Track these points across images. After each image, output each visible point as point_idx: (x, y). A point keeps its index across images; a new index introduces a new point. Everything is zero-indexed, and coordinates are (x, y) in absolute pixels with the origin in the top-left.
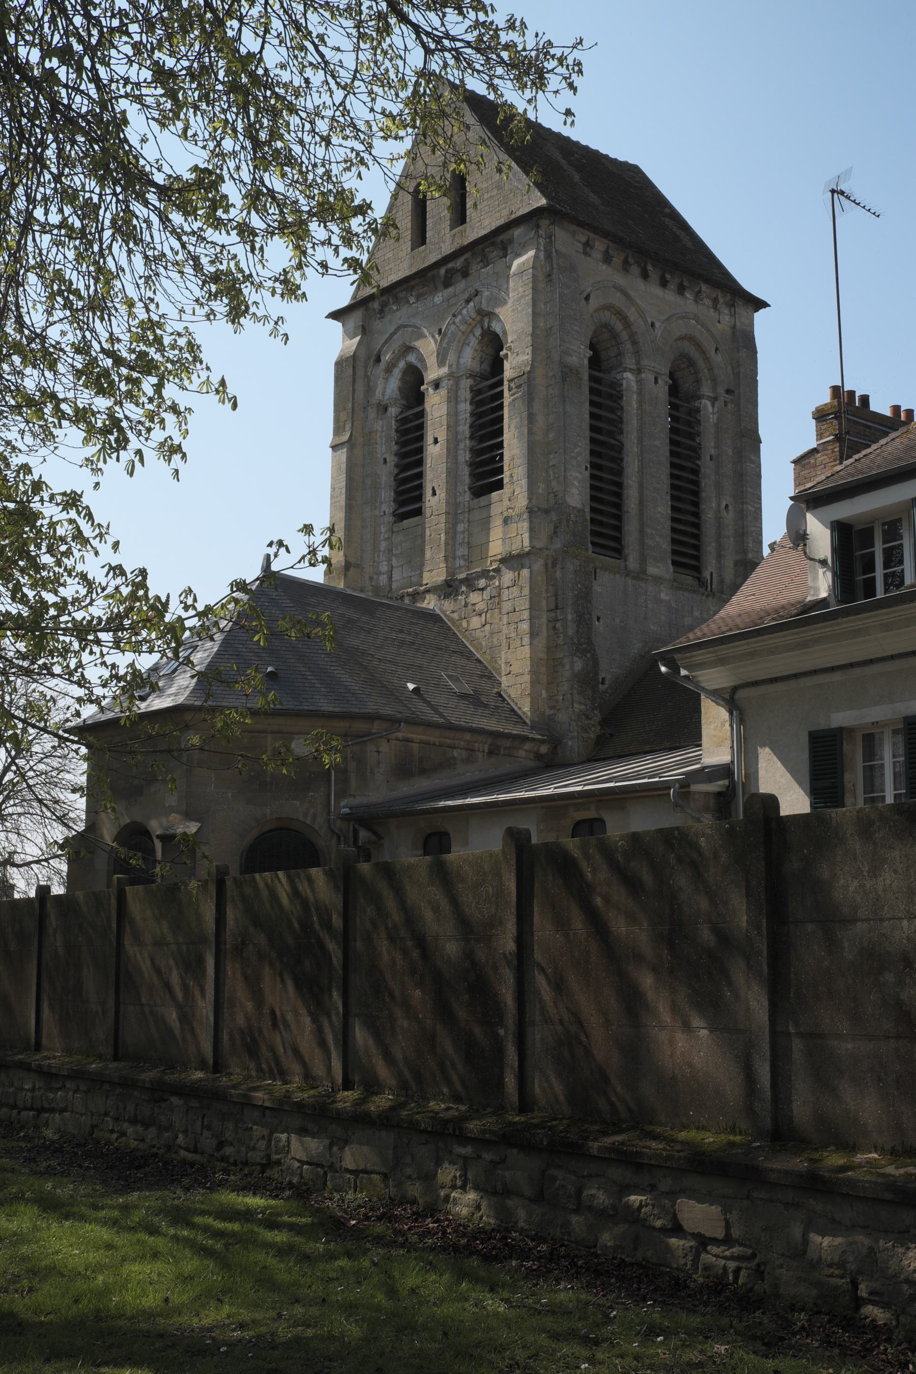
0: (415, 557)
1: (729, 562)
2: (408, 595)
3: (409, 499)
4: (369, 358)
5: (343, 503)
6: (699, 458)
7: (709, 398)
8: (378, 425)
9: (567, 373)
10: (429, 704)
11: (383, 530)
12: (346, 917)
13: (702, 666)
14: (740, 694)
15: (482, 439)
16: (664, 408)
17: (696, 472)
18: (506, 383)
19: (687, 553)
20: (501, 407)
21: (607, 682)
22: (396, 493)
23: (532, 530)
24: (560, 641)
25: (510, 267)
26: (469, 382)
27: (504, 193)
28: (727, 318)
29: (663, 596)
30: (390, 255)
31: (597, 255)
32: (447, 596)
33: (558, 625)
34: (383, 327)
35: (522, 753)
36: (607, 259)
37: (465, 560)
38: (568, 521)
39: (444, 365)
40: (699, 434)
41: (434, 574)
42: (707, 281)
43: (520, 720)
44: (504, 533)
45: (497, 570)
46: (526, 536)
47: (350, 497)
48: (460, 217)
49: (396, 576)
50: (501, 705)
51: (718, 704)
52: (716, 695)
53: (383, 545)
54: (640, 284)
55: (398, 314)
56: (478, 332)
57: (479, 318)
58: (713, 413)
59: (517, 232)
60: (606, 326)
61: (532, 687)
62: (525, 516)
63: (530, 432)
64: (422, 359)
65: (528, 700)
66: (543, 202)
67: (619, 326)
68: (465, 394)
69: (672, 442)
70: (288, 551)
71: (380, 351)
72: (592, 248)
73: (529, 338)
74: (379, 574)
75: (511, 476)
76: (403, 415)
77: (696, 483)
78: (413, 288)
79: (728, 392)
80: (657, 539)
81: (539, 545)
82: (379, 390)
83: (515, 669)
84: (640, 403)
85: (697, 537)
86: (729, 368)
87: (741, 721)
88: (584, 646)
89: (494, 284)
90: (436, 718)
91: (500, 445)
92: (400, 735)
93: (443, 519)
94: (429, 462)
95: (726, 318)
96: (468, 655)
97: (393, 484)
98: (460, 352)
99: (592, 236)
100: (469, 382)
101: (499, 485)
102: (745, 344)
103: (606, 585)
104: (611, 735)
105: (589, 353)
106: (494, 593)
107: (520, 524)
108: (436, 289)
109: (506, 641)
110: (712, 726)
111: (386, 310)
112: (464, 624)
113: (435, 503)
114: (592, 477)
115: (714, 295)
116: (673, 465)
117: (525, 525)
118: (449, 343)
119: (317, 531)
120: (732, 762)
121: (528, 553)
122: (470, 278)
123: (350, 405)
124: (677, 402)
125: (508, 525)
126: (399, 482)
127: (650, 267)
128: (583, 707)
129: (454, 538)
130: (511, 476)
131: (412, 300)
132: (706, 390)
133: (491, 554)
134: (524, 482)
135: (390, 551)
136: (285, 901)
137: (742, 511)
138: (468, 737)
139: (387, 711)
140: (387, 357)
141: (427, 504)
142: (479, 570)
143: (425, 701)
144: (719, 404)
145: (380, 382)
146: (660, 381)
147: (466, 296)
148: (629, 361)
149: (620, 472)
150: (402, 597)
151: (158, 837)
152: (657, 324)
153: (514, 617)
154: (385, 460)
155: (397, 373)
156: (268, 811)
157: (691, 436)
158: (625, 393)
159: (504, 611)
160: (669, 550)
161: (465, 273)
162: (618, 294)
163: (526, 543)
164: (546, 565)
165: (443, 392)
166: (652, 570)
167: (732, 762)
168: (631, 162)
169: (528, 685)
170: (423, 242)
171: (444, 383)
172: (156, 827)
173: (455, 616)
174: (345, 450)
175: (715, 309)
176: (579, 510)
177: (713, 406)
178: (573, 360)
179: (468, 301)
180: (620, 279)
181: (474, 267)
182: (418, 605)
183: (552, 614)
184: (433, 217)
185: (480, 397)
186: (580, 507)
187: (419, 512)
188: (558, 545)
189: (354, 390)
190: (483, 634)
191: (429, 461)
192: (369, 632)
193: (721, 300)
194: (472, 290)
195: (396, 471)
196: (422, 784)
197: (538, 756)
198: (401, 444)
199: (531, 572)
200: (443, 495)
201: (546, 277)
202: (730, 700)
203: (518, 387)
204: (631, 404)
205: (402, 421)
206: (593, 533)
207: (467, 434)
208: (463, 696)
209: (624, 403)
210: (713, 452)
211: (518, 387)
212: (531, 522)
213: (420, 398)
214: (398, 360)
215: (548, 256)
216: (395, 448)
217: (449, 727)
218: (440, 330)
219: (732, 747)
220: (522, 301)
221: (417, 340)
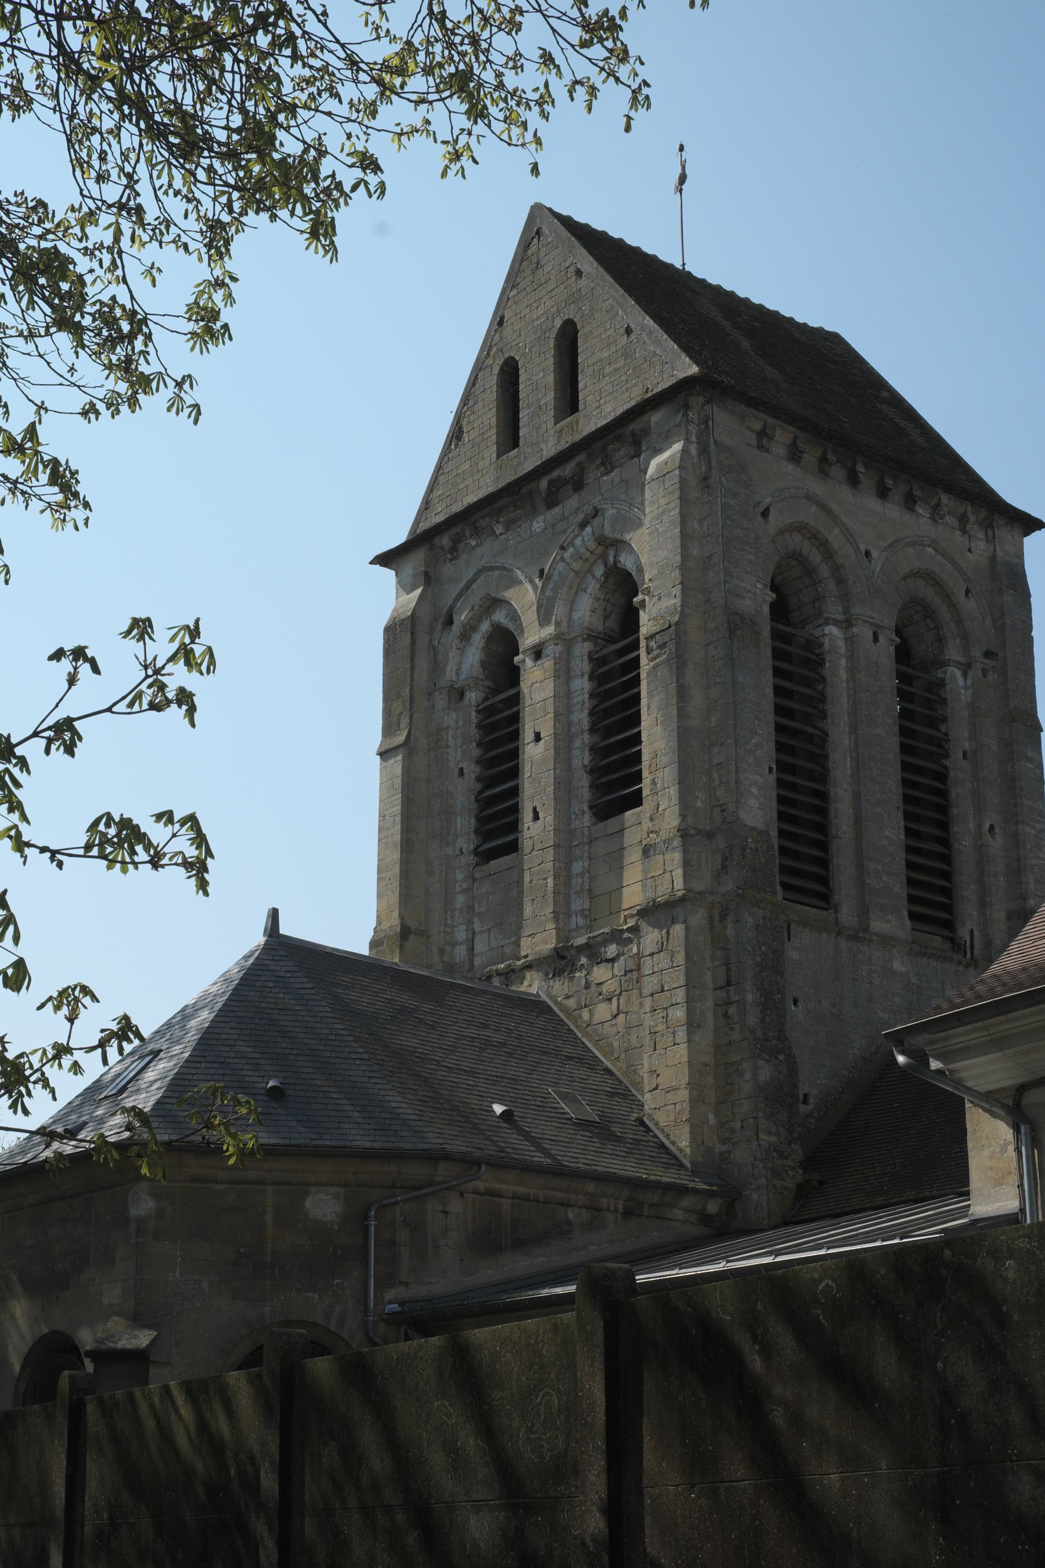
0: (509, 917)
1: (998, 912)
2: (499, 973)
3: (498, 827)
4: (436, 620)
5: (398, 838)
6: (946, 756)
7: (958, 665)
8: (450, 719)
9: (737, 625)
10: (527, 1136)
11: (460, 876)
12: (287, 1472)
13: (964, 1052)
14: (1032, 1097)
15: (608, 732)
16: (889, 683)
17: (942, 776)
18: (643, 644)
19: (932, 900)
20: (636, 681)
21: (811, 1100)
22: (478, 819)
23: (686, 864)
24: (736, 1036)
25: (645, 471)
26: (588, 646)
27: (633, 361)
28: (982, 545)
29: (897, 966)
30: (466, 466)
31: (779, 449)
32: (558, 973)
33: (732, 1011)
34: (457, 572)
35: (678, 1214)
36: (794, 455)
37: (586, 917)
38: (743, 849)
39: (548, 623)
40: (944, 720)
41: (539, 939)
42: (949, 489)
43: (673, 1161)
44: (645, 871)
45: (635, 930)
46: (678, 873)
47: (407, 829)
48: (569, 401)
49: (480, 946)
50: (644, 1137)
51: (994, 1115)
52: (991, 1100)
53: (460, 900)
54: (846, 493)
55: (479, 551)
56: (599, 571)
57: (600, 549)
58: (966, 688)
59: (655, 418)
60: (796, 555)
61: (692, 1108)
62: (676, 842)
63: (682, 714)
64: (515, 617)
65: (687, 1129)
66: (694, 369)
67: (815, 557)
68: (581, 664)
69: (903, 731)
70: (96, 670)
71: (451, 608)
72: (771, 439)
73: (677, 572)
74: (454, 944)
75: (654, 782)
76: (488, 703)
77: (944, 794)
78: (499, 511)
79: (988, 654)
80: (885, 878)
81: (698, 886)
82: (451, 667)
83: (664, 1081)
84: (852, 671)
85: (946, 875)
86: (988, 619)
87: (1034, 1142)
88: (774, 1042)
89: (623, 497)
90: (539, 1158)
91: (637, 739)
92: (481, 1185)
93: (550, 854)
94: (527, 771)
95: (980, 545)
96: (592, 1063)
97: (474, 806)
98: (573, 602)
99: (770, 420)
100: (588, 646)
101: (636, 800)
102: (1012, 584)
103: (805, 949)
104: (821, 1183)
105: (771, 596)
106: (631, 965)
107: (668, 856)
109: (651, 1038)
110: (986, 1153)
111: (461, 546)
112: (585, 1015)
113: (537, 831)
114: (780, 783)
115: (961, 511)
116: (905, 766)
117: (677, 856)
118: (555, 590)
119: (161, 632)
120: (1022, 1210)
121: (682, 900)
123: (407, 690)
124: (909, 671)
125: (650, 856)
126: (485, 803)
127: (860, 468)
128: (773, 1139)
129: (567, 883)
130: (654, 782)
131: (499, 529)
132: (953, 652)
133: (625, 906)
134: (673, 791)
135: (470, 908)
136: (182, 1440)
138: (591, 1187)
139: (458, 1146)
140: (462, 617)
141: (526, 834)
142: (606, 930)
143: (521, 1131)
144: (974, 673)
145: (453, 653)
146: (882, 639)
147: (580, 517)
148: (834, 609)
149: (824, 777)
150: (489, 978)
151: (88, 1354)
152: (875, 554)
153: (662, 1000)
155: (478, 639)
157: (933, 722)
158: (828, 658)
159: (646, 991)
160: (904, 895)
162: (814, 508)
163: (679, 884)
164: (711, 918)
165: (547, 663)
166: (878, 926)
167: (1022, 1210)
168: (829, 328)
169: (686, 1105)
170: (515, 444)
171: (549, 650)
172: (86, 1338)
173: (571, 1003)
174: (400, 757)
175: (964, 531)
176: (761, 833)
177: (965, 676)
178: (746, 605)
179: (583, 525)
180: (817, 487)
181: (591, 477)
182: (514, 988)
183: (722, 994)
184: (529, 406)
185: (605, 668)
186: (761, 826)
187: (513, 847)
188: (728, 886)
189: (413, 668)
190: (614, 1030)
191: (527, 768)
192: (433, 1027)
193: (972, 518)
194: (588, 509)
195: (478, 787)
196: (518, 1264)
197: (705, 1219)
198: (485, 745)
199: (687, 929)
200: (550, 819)
201: (698, 482)
202: (1014, 1106)
203: (662, 646)
204: (838, 671)
205: (486, 711)
206: (783, 869)
207: (586, 724)
208: (584, 1124)
209: (826, 671)
210: (967, 746)
211: (662, 646)
212: (685, 852)
213: (513, 676)
214: (480, 621)
215: (704, 450)
216: (476, 752)
217: (560, 1172)
218: (542, 571)
219: (1021, 1186)
220: (665, 518)
221: (508, 587)
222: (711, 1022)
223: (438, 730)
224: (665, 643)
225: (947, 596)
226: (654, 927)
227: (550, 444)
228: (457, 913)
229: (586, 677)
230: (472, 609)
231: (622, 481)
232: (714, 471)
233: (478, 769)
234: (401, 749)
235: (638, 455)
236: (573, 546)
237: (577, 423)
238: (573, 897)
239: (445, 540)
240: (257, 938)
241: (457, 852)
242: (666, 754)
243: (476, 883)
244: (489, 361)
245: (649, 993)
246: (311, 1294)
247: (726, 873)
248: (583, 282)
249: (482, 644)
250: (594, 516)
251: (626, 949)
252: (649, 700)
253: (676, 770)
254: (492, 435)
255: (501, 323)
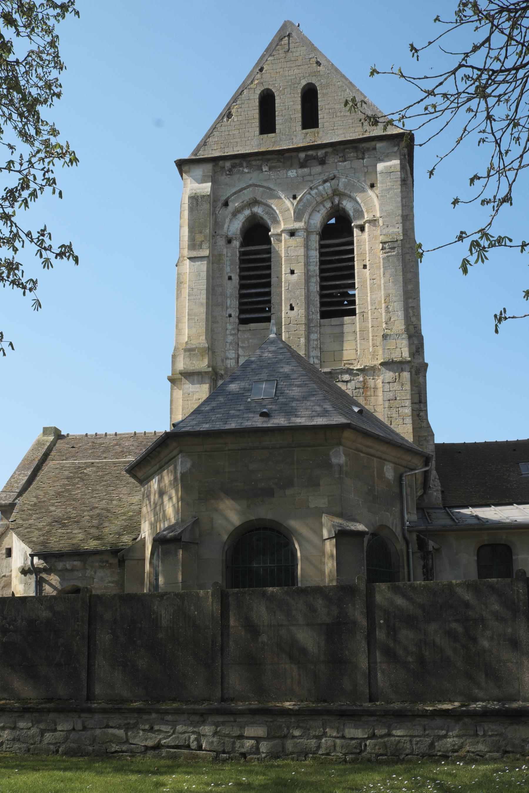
56: (328, 205)
71: (228, 198)
78: (269, 160)
108: (291, 167)
122: (325, 166)
140: (235, 204)
179: (325, 182)
181: (331, 160)
183: (417, 406)
224: (395, 247)
226: (390, 370)
227: (298, 138)
228: (228, 344)
230: (243, 202)
231: (351, 168)
234: (206, 259)
235: (363, 159)
236: (317, 189)
237: (318, 133)
239: (228, 164)
241: (227, 315)
242: (396, 296)
243: (240, 333)
245: (387, 399)
247: (419, 355)
248: (321, 68)
249: (243, 220)
250: (333, 179)
251: (355, 378)
252: (384, 270)
253: (402, 305)
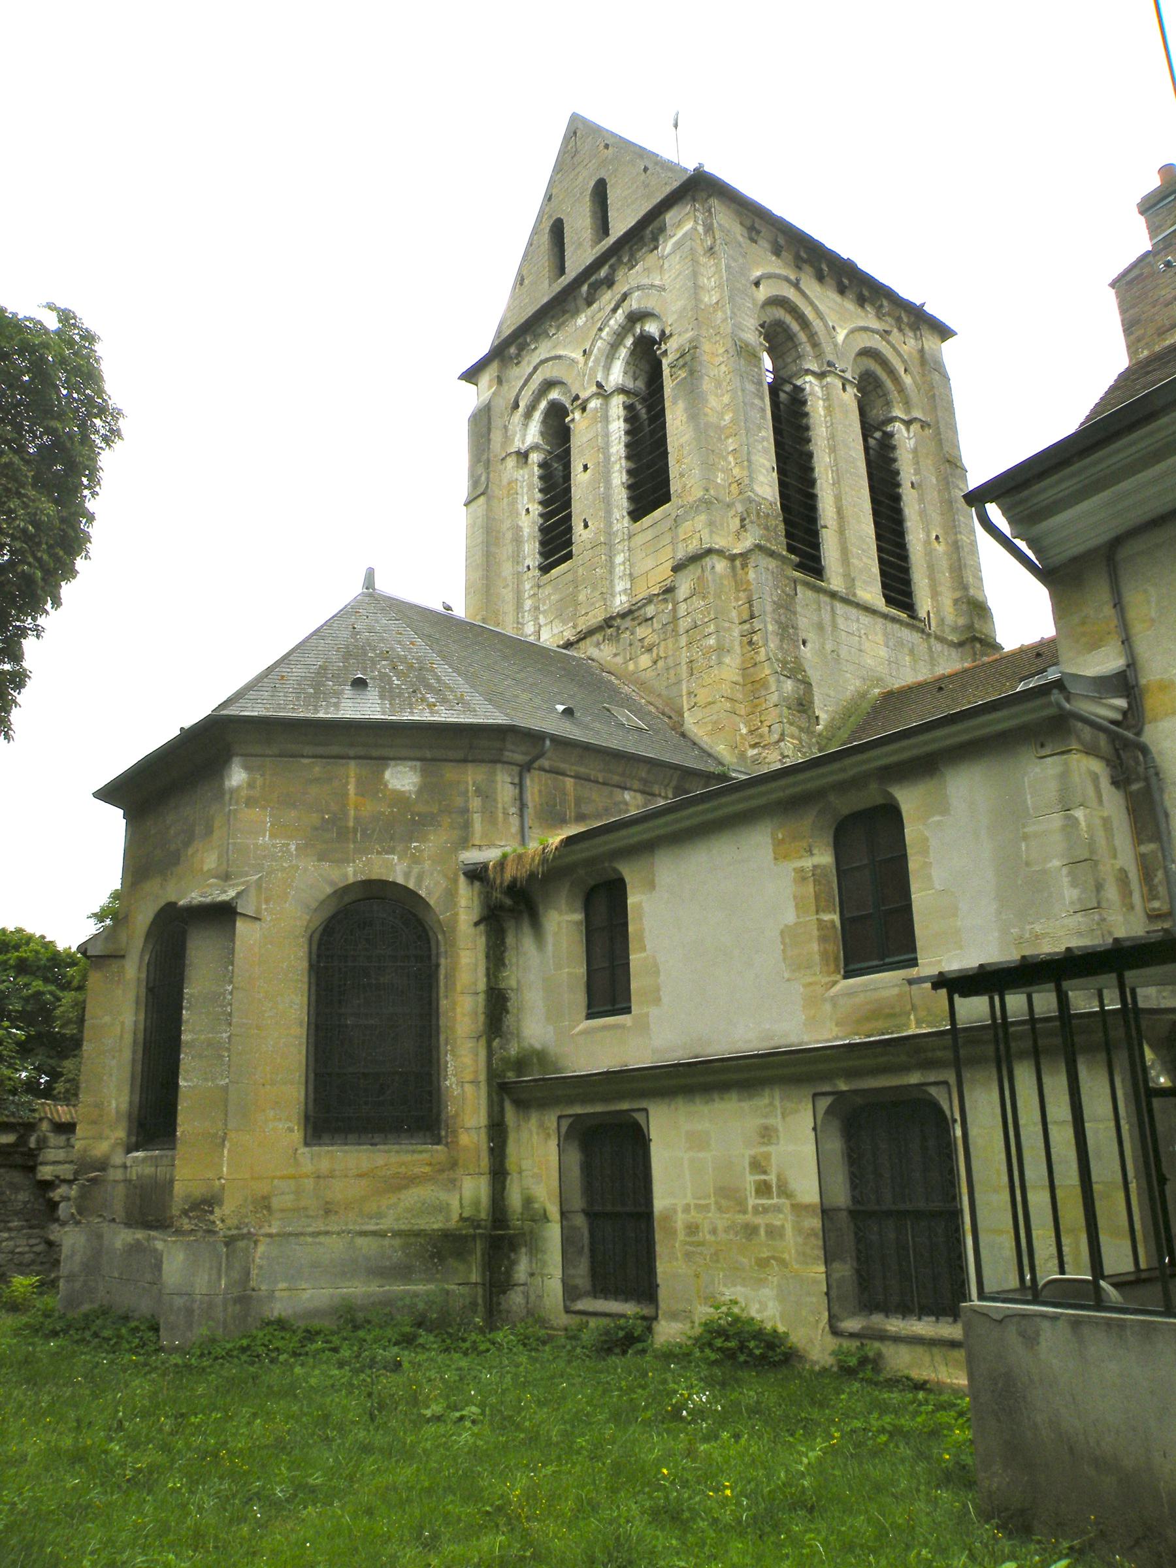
11: (527, 586)
28: (912, 341)
48: (603, 227)
53: (528, 604)
95: (912, 342)
97: (537, 534)
135: (537, 608)
137: (956, 542)
147: (612, 306)
154: (528, 510)
155: (538, 416)
156: (350, 870)
159: (682, 631)
161: (609, 282)
177: (908, 430)
207: (623, 453)
209: (808, 409)
222: (737, 648)
223: (509, 483)
225: (891, 372)
229: (622, 420)
232: (718, 242)
233: (540, 508)
238: (616, 581)
240: (355, 589)
244: (542, 227)
246: (391, 856)
254: (546, 272)
255: (550, 199)
